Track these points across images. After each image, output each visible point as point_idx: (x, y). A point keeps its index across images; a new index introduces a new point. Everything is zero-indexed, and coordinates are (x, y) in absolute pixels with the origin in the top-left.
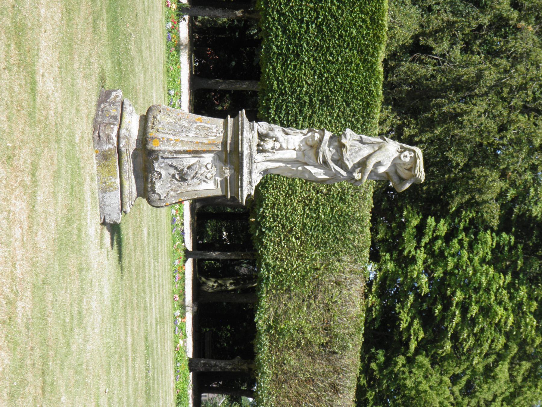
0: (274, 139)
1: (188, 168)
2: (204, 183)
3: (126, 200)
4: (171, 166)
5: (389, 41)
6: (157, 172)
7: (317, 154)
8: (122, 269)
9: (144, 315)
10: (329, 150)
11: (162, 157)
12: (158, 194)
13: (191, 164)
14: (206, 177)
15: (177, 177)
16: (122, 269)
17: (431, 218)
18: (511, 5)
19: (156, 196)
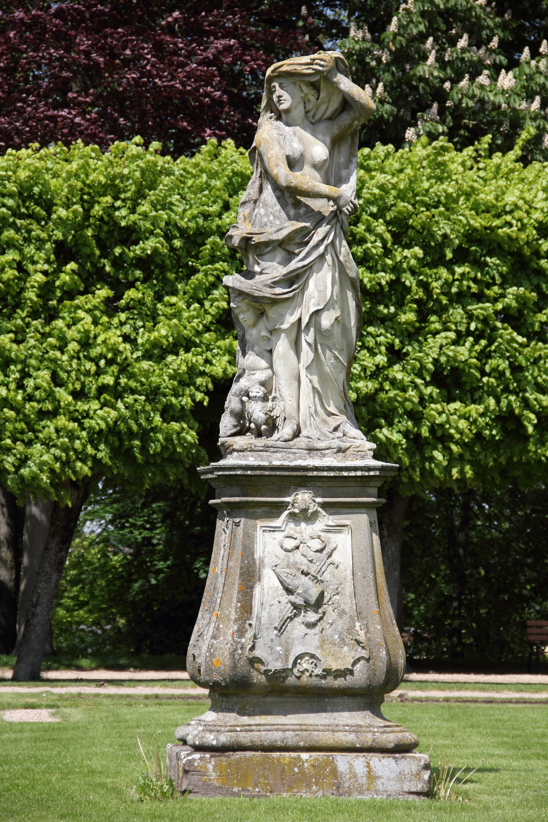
0: (245, 399)
1: (289, 591)
2: (335, 557)
3: (368, 739)
4: (281, 630)
5: (262, 671)
6: (295, 663)
7: (274, 301)
8: (333, 551)
9: (138, 357)
10: (261, 273)
11: (253, 648)
12: (354, 664)
13: (281, 587)
14: (321, 551)
15: (312, 617)
16: (333, 551)
17: (507, 72)
18: (103, 384)
19: (358, 666)
